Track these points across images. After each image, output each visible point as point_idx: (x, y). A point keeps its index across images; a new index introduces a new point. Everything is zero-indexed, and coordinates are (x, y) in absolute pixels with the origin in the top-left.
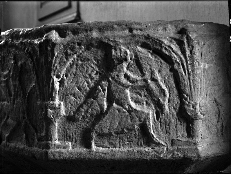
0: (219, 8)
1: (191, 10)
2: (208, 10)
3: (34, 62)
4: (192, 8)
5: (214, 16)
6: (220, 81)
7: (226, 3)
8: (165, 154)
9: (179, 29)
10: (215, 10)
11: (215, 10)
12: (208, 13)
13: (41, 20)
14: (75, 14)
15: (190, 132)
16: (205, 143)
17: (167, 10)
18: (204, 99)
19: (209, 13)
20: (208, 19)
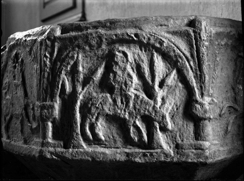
1: (203, 10)
2: (221, 10)
4: (203, 9)
11: (228, 11)
12: (220, 13)
14: (80, 15)
15: (198, 134)
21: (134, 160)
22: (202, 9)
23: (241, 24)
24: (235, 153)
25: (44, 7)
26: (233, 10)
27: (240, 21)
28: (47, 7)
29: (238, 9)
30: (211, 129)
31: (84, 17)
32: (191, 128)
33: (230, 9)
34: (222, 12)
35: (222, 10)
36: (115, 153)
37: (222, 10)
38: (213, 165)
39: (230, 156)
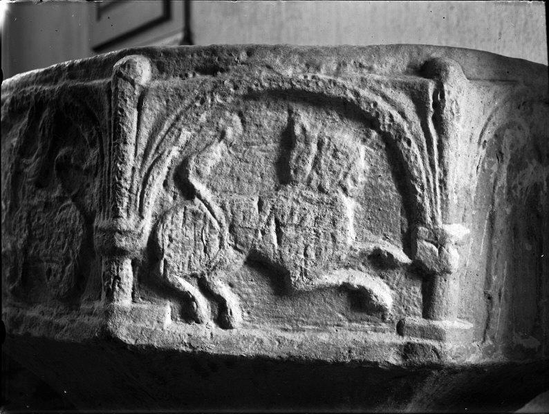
0: (523, 22)
1: (458, 25)
2: (498, 25)
3: (73, 126)
4: (458, 22)
5: (512, 41)
6: (515, 298)
7: (540, 11)
8: (311, 90)
9: (421, 61)
10: (515, 27)
11: (515, 27)
12: (498, 32)
13: (99, 49)
14: (180, 36)
15: (429, 307)
16: (460, 334)
17: (399, 26)
18: (463, 238)
19: (500, 34)
20: (499, 47)
21: (33, 176)
22: (455, 22)
23: (543, 81)
24: (499, 357)
25: (99, 17)
26: (526, 23)
27: (540, 66)
28: (105, 17)
29: (537, 21)
30: (455, 291)
31: (188, 38)
32: (416, 291)
33: (519, 23)
34: (502, 28)
35: (501, 23)
36: (251, 331)
37: (501, 23)
38: (453, 370)
39: (487, 360)
